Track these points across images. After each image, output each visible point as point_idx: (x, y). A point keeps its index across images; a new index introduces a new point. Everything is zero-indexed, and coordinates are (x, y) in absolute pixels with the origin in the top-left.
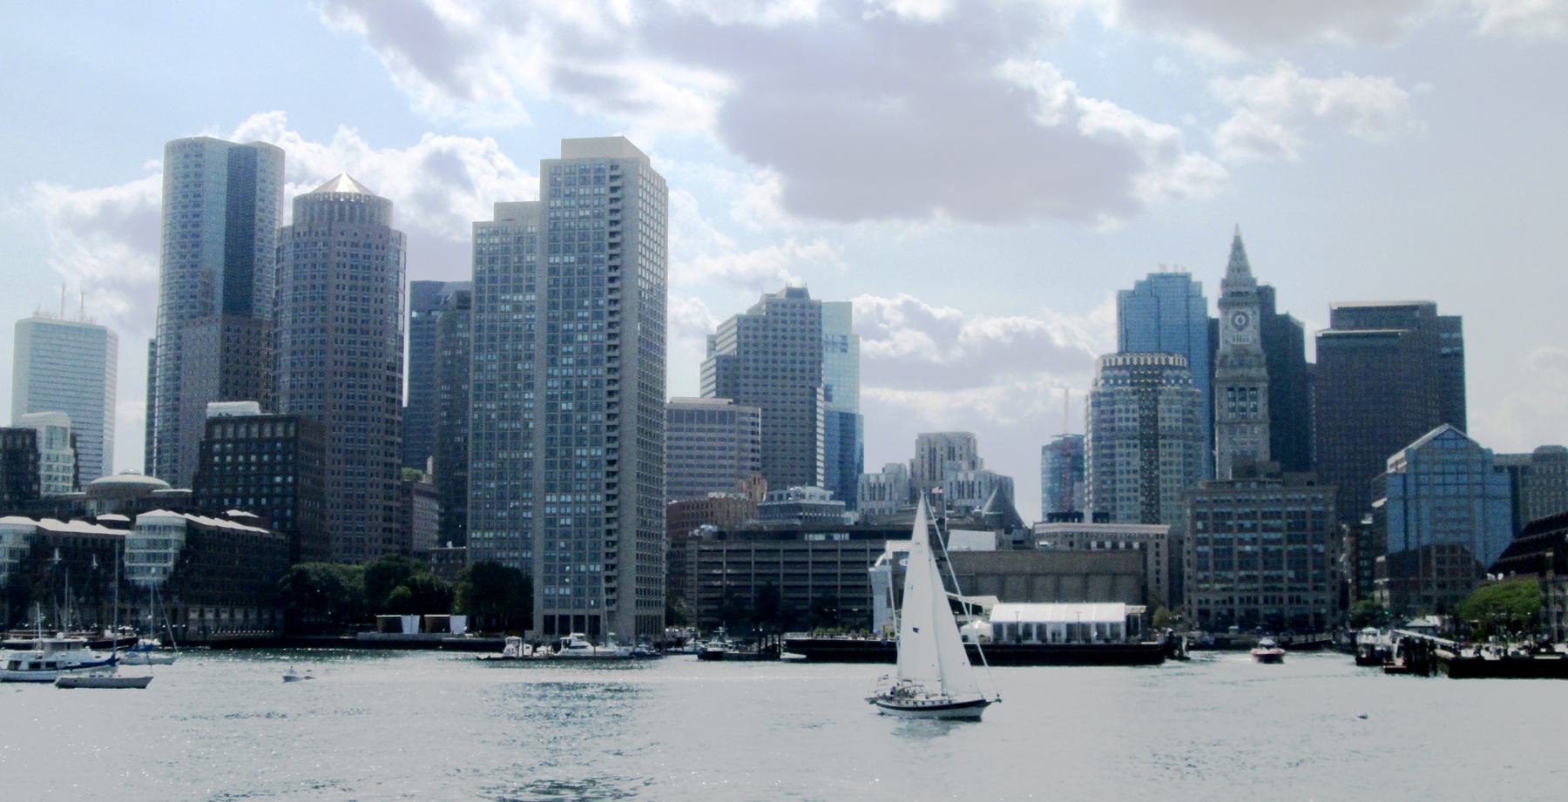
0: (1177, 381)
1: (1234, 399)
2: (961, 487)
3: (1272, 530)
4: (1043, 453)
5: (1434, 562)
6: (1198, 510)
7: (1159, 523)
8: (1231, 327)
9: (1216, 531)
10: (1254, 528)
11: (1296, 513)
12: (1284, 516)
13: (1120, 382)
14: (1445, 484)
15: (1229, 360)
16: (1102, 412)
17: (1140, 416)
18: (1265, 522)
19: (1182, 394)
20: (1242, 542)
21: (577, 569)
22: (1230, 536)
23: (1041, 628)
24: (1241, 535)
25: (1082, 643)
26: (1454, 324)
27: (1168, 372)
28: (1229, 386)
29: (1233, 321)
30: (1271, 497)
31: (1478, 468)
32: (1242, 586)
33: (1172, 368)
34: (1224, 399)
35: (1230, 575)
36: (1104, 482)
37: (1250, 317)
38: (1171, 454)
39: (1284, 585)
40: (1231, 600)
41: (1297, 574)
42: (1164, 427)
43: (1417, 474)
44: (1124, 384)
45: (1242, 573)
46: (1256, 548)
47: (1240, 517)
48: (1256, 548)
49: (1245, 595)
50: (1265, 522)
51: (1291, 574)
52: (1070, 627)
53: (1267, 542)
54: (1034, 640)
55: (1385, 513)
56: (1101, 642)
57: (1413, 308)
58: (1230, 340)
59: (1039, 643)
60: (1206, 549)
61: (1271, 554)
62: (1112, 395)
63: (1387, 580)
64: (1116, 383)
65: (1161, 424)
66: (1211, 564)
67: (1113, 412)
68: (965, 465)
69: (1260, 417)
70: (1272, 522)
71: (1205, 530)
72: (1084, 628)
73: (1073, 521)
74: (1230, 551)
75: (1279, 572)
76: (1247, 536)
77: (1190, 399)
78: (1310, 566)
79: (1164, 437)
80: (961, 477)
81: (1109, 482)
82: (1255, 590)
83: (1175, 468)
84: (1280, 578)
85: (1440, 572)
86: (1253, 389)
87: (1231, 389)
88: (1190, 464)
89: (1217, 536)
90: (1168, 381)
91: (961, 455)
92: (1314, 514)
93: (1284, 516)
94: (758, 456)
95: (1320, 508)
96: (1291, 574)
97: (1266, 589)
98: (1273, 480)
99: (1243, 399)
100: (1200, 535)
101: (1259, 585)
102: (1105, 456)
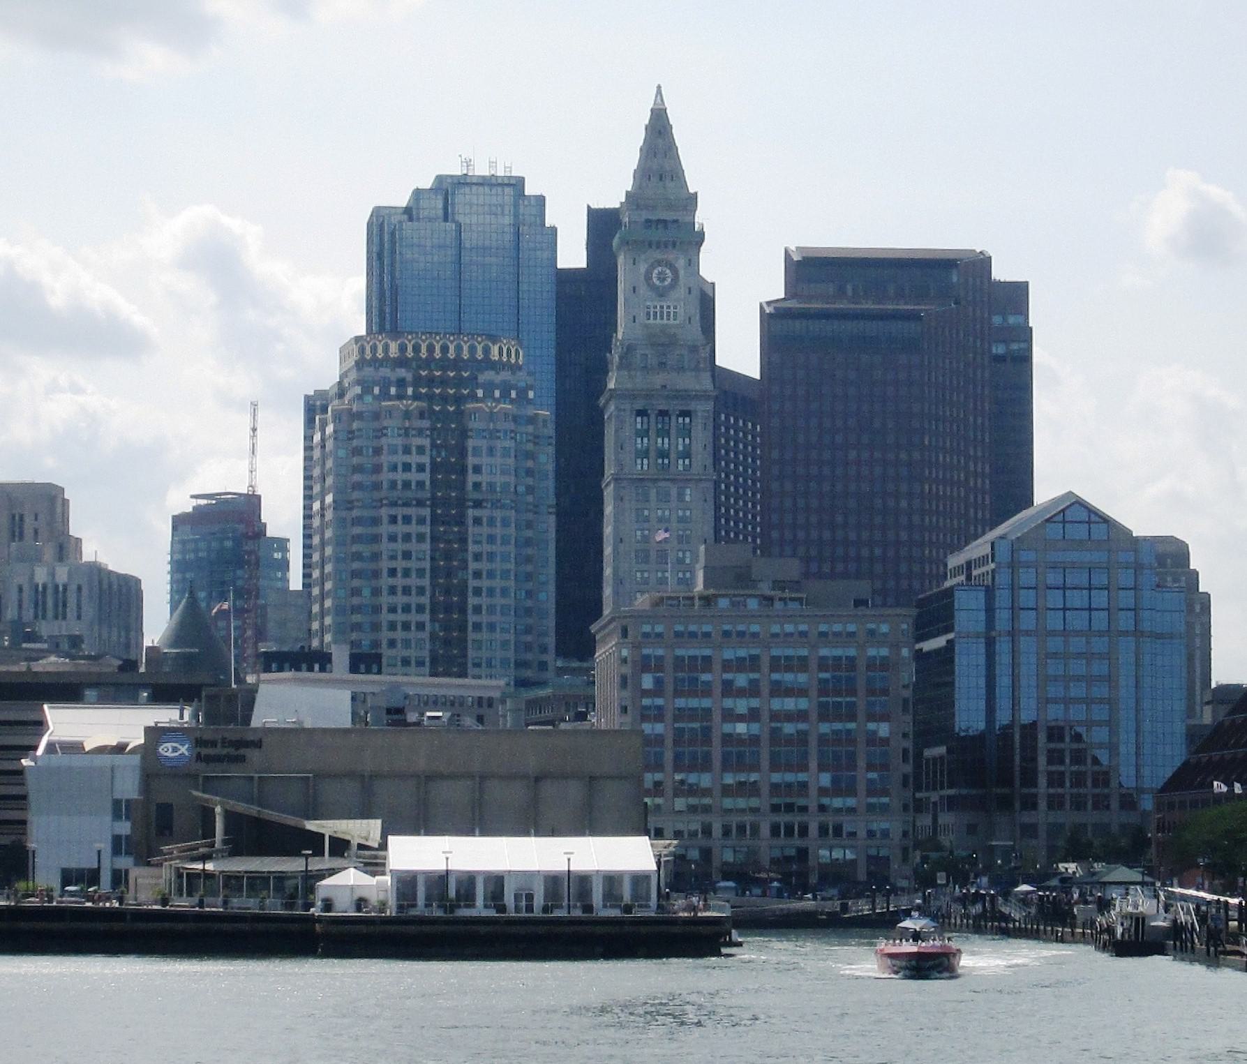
0: (505, 395)
1: (644, 433)
2: (39, 595)
3: (789, 692)
4: (174, 528)
5: (1042, 760)
6: (646, 651)
7: (463, 674)
8: (643, 290)
9: (678, 693)
10: (753, 690)
11: (837, 659)
12: (813, 665)
14: (1090, 609)
15: (639, 352)
16: (357, 451)
17: (433, 463)
18: (775, 676)
19: (515, 419)
20: (730, 716)
22: (706, 703)
23: (496, 882)
24: (728, 703)
25: (577, 913)
26: (1017, 295)
29: (648, 277)
30: (789, 628)
31: (1126, 578)
32: (728, 803)
34: (628, 432)
35: (705, 780)
36: (356, 592)
37: (682, 273)
38: (491, 539)
39: (812, 802)
40: (707, 831)
41: (835, 781)
42: (477, 486)
45: (729, 779)
46: (755, 728)
47: (727, 666)
48: (755, 728)
49: (734, 820)
50: (775, 676)
51: (825, 779)
53: (775, 716)
54: (480, 909)
55: (952, 661)
56: (614, 913)
58: (641, 318)
59: (492, 913)
60: (659, 728)
61: (789, 740)
62: (376, 416)
64: (385, 395)
65: (471, 478)
66: (669, 756)
67: (378, 451)
68: (49, 553)
69: (697, 468)
70: (788, 677)
71: (658, 690)
72: (583, 881)
73: (311, 669)
74: (707, 732)
75: (802, 777)
76: (742, 706)
77: (530, 429)
78: (861, 763)
79: (478, 504)
80: (41, 576)
81: (366, 592)
82: (755, 810)
83: (498, 565)
84: (804, 786)
85: (1056, 780)
86: (685, 414)
87: (641, 413)
88: (528, 560)
89: (681, 702)
90: (489, 395)
91: (36, 532)
92: (871, 664)
93: (813, 665)
95: (884, 652)
96: (825, 779)
97: (775, 808)
98: (787, 594)
99: (664, 433)
100: (646, 702)
101: (761, 802)
102: (357, 539)
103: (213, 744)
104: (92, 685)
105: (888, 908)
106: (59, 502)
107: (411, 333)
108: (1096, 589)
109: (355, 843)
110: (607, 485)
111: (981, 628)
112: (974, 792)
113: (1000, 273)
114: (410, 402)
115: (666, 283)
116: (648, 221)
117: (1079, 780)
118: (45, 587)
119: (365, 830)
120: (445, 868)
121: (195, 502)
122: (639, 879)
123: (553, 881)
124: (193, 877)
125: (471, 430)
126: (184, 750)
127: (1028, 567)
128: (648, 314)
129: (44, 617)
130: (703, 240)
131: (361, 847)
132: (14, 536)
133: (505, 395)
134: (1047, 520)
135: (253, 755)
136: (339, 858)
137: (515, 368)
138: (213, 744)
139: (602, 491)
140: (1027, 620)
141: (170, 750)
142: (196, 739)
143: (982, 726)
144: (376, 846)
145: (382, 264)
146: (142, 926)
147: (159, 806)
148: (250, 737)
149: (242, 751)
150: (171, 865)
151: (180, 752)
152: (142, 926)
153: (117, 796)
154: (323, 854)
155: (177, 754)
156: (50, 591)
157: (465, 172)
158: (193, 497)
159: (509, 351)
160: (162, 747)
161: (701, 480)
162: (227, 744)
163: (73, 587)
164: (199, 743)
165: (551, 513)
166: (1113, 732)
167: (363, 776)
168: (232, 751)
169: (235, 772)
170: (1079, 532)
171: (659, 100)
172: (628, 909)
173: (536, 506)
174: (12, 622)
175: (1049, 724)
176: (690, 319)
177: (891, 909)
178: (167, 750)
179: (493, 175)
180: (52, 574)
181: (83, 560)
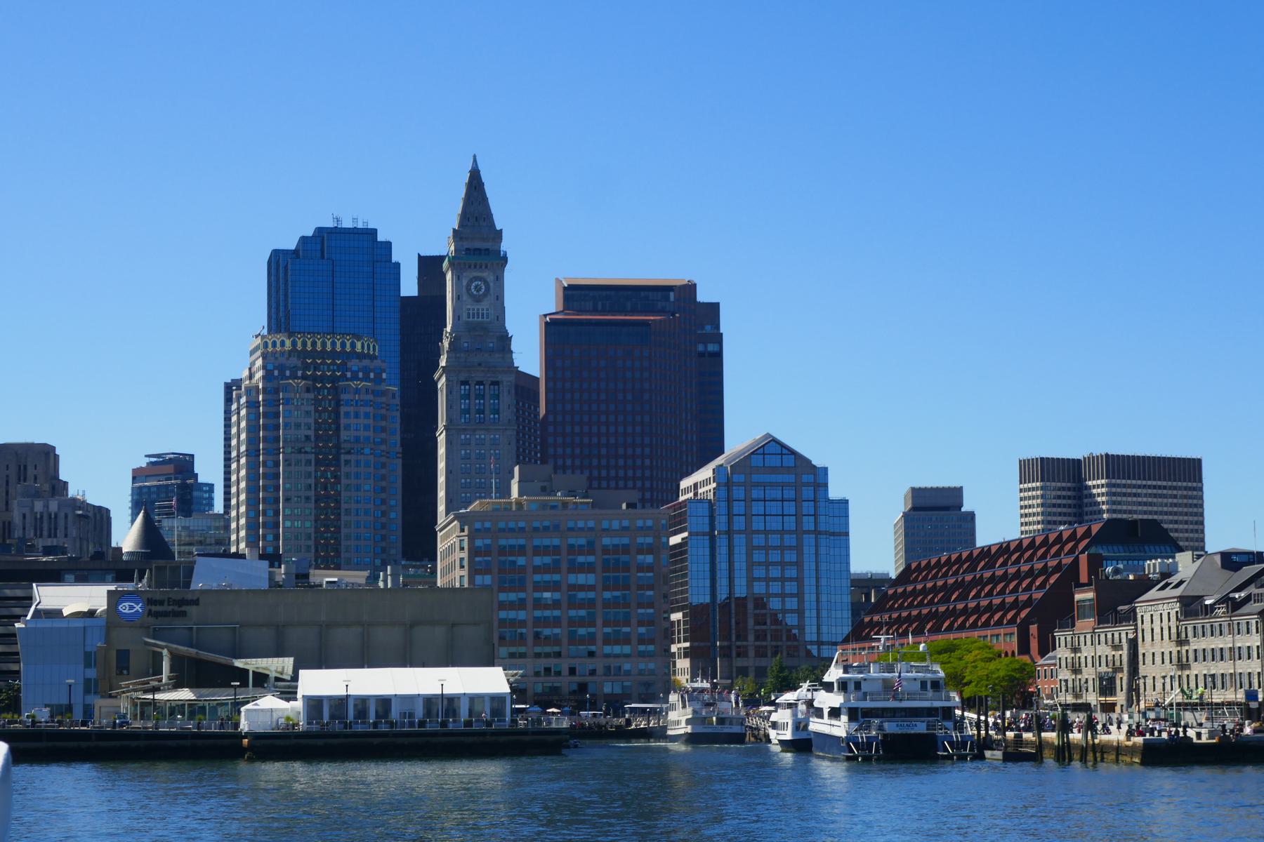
2: (38, 521)
5: (751, 622)
7: (339, 569)
8: (465, 297)
13: (288, 373)
17: (316, 422)
21: (299, 499)
23: (385, 702)
27: (354, 364)
28: (462, 378)
29: (468, 289)
33: (361, 356)
37: (491, 285)
43: (729, 501)
44: (294, 377)
46: (557, 596)
52: (429, 701)
57: (665, 289)
58: (465, 316)
63: (687, 644)
65: (344, 435)
85: (760, 636)
94: (278, 348)
95: (649, 540)
103: (161, 603)
104: (70, 571)
105: (659, 724)
106: (52, 455)
107: (299, 333)
108: (786, 501)
109: (273, 675)
110: (440, 435)
111: (707, 529)
112: (702, 644)
113: (703, 296)
114: (299, 381)
115: (481, 293)
116: (467, 249)
117: (776, 637)
118: (42, 517)
119: (281, 665)
120: (345, 693)
121: (148, 460)
122: (497, 699)
123: (429, 701)
124: (146, 704)
125: (343, 400)
126: (138, 608)
127: (739, 486)
128: (469, 314)
129: (41, 536)
130: (506, 262)
131: (277, 679)
132: (19, 479)
133: (366, 378)
134: (752, 453)
135: (192, 610)
136: (260, 688)
137: (373, 358)
138: (161, 603)
139: (436, 438)
140: (739, 523)
141: (128, 608)
142: (148, 599)
143: (707, 599)
144: (289, 678)
145: (278, 281)
146: (103, 744)
147: (118, 651)
148: (189, 597)
149: (183, 608)
150: (128, 697)
151: (135, 610)
152: (103, 744)
153: (88, 649)
154: (248, 686)
155: (133, 611)
156: (45, 517)
157: (336, 225)
158: (146, 456)
159: (368, 345)
160: (121, 606)
161: (506, 429)
162: (171, 603)
163: (62, 515)
164: (150, 602)
165: (397, 458)
166: (801, 602)
167: (278, 626)
168: (176, 608)
169: (179, 623)
170: (774, 461)
171: (474, 165)
172: (489, 724)
173: (388, 453)
174: (19, 538)
175: (755, 596)
176: (498, 317)
177: (661, 725)
178: (125, 608)
179: (355, 228)
180: (46, 506)
181: (69, 497)
